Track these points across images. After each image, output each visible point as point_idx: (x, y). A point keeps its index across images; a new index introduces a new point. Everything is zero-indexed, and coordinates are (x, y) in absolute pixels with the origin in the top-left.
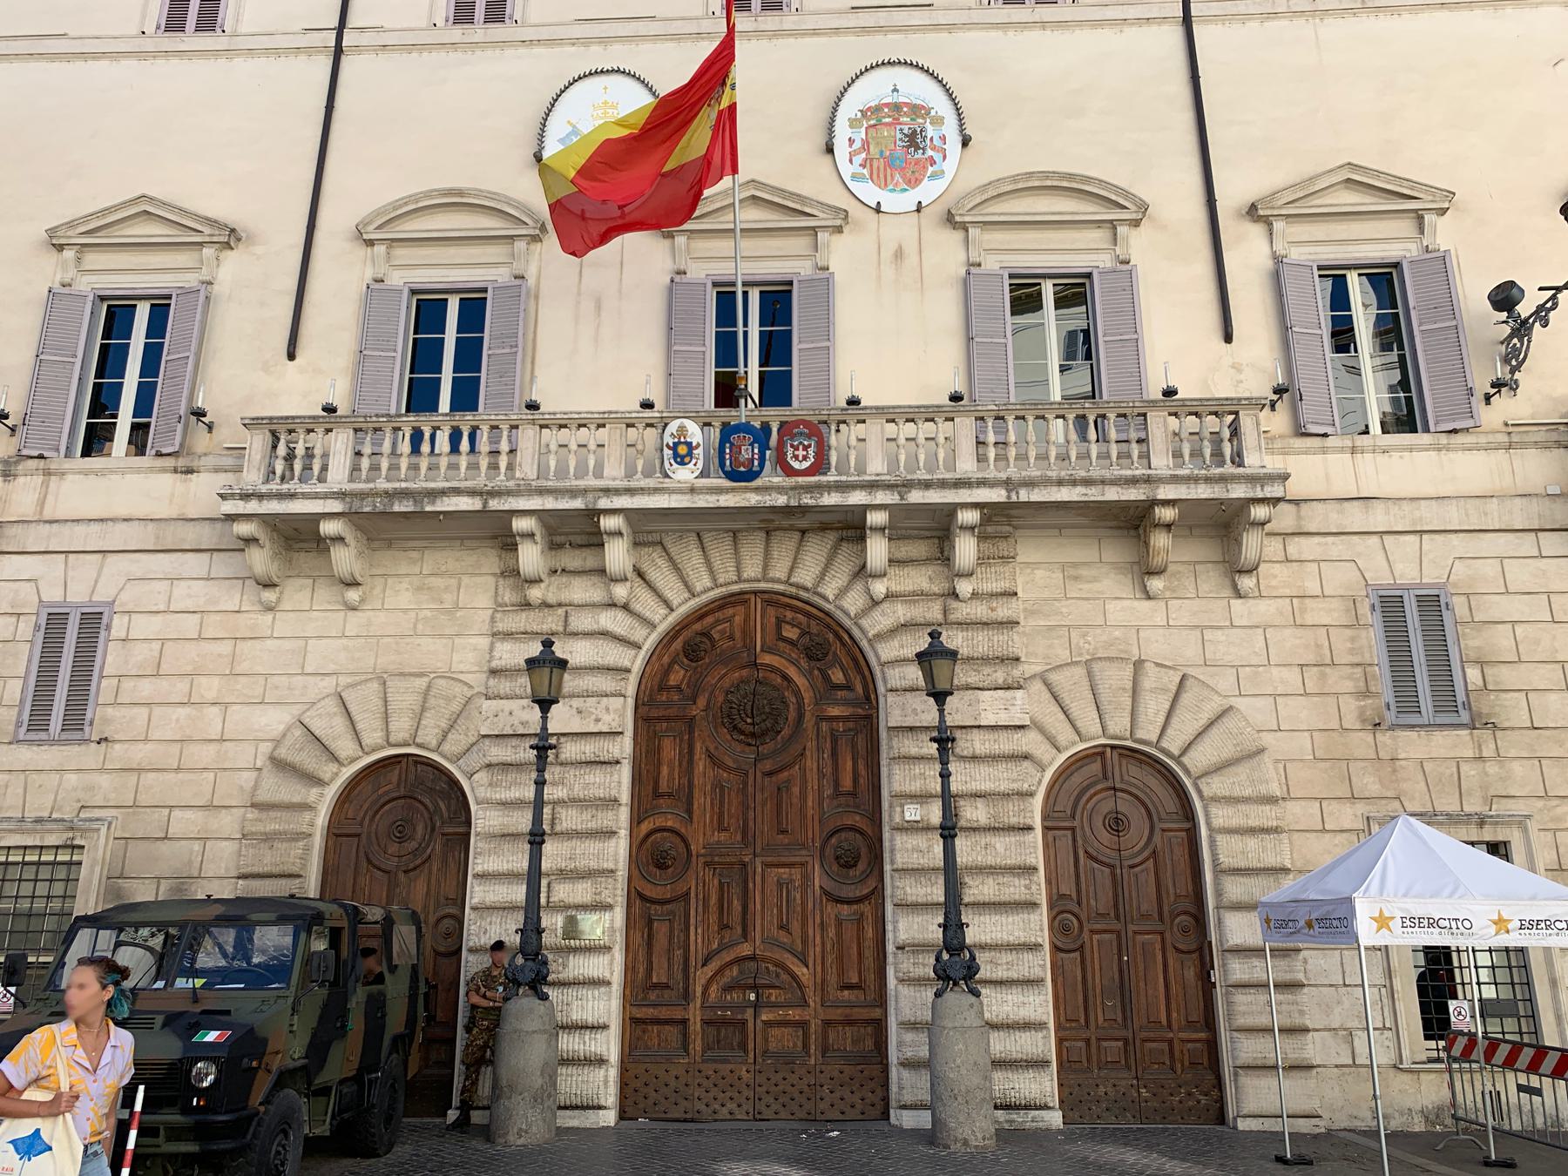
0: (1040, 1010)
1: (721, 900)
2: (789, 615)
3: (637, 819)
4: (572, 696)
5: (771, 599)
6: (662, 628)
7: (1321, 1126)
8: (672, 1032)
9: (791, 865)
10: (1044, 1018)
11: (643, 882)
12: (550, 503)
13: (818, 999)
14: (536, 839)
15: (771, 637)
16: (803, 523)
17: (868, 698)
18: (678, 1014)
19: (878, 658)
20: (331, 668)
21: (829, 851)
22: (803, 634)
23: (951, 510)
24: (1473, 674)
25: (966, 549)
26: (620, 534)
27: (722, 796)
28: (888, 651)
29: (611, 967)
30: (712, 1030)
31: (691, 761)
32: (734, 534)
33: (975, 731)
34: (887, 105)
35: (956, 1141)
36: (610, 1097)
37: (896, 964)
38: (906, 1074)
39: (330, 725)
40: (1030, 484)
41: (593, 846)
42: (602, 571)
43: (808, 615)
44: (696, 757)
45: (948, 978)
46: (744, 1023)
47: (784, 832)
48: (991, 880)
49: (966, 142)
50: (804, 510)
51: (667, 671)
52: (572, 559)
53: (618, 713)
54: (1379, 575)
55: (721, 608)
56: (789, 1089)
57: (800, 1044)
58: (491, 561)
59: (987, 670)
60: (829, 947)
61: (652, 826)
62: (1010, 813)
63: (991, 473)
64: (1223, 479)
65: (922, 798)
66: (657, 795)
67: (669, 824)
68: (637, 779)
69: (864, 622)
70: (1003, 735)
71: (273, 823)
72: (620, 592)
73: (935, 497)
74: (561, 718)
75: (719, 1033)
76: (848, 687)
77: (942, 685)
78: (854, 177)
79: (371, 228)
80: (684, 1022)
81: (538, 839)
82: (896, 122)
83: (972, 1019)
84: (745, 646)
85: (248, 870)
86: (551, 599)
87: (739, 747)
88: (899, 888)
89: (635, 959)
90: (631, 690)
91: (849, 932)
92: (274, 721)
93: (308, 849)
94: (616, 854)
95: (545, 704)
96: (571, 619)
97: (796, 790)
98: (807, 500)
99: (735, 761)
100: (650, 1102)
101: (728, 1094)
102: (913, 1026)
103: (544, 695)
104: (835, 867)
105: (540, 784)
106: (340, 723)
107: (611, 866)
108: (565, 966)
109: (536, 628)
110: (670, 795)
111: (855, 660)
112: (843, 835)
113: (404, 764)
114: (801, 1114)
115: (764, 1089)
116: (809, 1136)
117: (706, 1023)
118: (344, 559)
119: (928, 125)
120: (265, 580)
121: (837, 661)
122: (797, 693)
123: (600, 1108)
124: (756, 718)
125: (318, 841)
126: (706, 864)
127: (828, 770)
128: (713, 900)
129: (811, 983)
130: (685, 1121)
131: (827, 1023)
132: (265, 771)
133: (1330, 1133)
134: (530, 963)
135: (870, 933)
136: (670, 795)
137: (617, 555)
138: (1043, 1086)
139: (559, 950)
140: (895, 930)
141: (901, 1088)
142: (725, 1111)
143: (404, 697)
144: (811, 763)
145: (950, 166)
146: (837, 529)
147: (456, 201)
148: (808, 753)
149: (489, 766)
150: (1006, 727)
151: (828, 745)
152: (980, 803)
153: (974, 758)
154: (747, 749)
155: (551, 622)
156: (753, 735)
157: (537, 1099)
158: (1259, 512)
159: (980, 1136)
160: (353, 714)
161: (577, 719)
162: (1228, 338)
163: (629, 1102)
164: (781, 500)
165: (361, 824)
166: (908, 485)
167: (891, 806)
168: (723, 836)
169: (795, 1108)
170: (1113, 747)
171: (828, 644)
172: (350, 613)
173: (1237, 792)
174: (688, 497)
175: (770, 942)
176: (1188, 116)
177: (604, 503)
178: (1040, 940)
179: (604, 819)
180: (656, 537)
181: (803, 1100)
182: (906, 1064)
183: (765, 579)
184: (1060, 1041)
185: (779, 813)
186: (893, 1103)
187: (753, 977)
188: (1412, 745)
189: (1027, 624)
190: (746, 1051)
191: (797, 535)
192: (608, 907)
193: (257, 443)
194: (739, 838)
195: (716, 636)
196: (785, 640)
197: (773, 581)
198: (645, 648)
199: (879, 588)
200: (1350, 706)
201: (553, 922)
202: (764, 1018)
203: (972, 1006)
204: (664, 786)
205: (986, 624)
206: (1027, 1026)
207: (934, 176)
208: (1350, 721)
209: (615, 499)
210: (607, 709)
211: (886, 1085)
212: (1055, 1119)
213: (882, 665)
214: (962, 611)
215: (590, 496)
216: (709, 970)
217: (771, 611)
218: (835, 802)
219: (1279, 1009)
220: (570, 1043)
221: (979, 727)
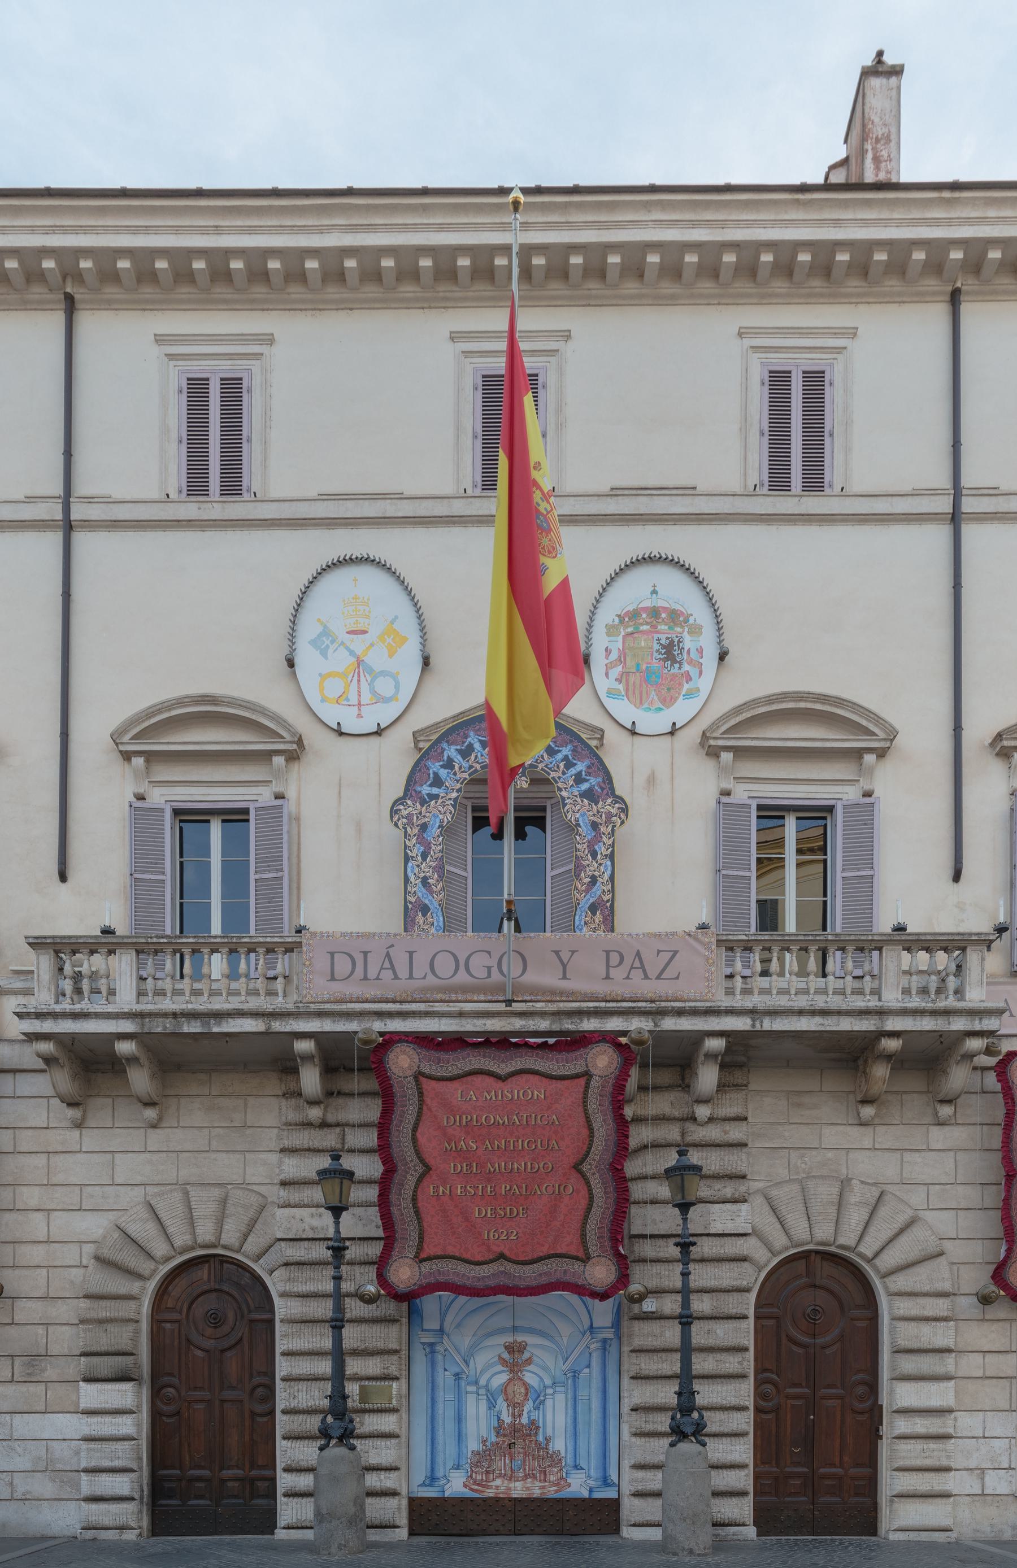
0: (745, 1455)
7: (953, 1536)
10: (747, 1461)
12: (327, 1026)
20: (138, 1179)
25: (707, 1077)
33: (704, 1238)
34: (645, 609)
36: (403, 1520)
39: (144, 1230)
40: (774, 1013)
58: (274, 1085)
62: (731, 1304)
63: (739, 1001)
64: (947, 1013)
71: (105, 1310)
73: (685, 1024)
78: (611, 693)
79: (126, 738)
82: (654, 629)
85: (88, 1349)
86: (331, 1118)
92: (94, 1226)
93: (137, 1332)
95: (337, 1211)
106: (151, 1227)
108: (362, 1424)
113: (212, 1262)
118: (140, 1080)
119: (687, 637)
120: (146, 1100)
123: (398, 1527)
125: (145, 1326)
132: (91, 1267)
133: (957, 1542)
138: (743, 1509)
143: (205, 1205)
145: (705, 683)
149: (287, 1264)
153: (702, 1260)
159: (702, 1547)
160: (163, 1219)
162: (957, 877)
165: (180, 1313)
166: (663, 1013)
170: (817, 1252)
172: (150, 1131)
173: (918, 1288)
176: (944, 635)
178: (747, 1403)
184: (757, 1478)
189: (756, 1144)
193: (44, 964)
201: (352, 1389)
203: (700, 1453)
206: (732, 1466)
207: (690, 694)
209: (388, 1022)
212: (750, 1532)
219: (934, 1453)
220: (372, 1480)
221: (708, 1235)
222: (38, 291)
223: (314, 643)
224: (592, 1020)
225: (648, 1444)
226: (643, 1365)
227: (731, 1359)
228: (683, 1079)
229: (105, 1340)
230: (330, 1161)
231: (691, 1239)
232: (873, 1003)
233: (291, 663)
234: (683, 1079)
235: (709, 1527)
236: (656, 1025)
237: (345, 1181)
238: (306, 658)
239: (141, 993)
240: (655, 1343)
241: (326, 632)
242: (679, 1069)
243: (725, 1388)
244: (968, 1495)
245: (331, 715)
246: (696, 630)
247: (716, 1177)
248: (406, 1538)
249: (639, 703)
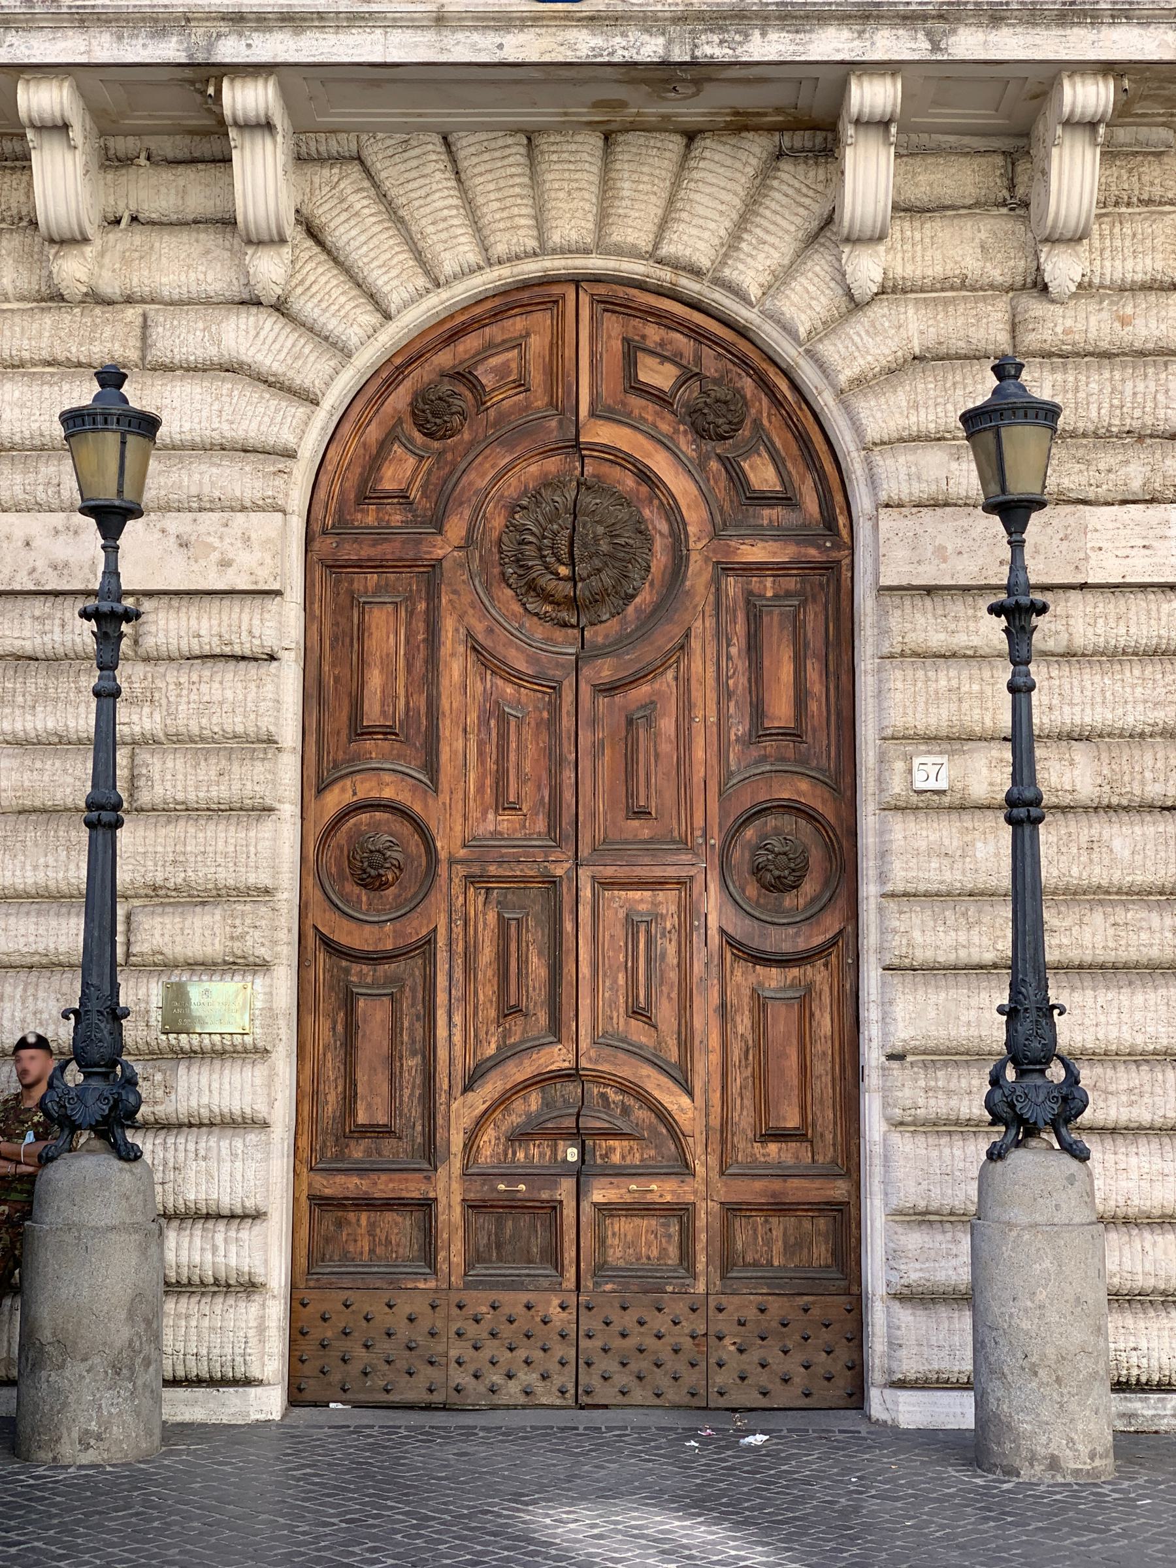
1: (502, 958)
2: (654, 334)
3: (316, 782)
4: (165, 508)
5: (615, 297)
6: (367, 358)
8: (400, 1229)
9: (658, 884)
11: (333, 917)
12: (104, 48)
13: (713, 1161)
14: (103, 816)
15: (612, 385)
16: (691, 112)
17: (830, 524)
18: (413, 1188)
19: (857, 428)
21: (738, 855)
22: (688, 376)
23: (1044, 80)
25: (1073, 176)
26: (267, 126)
27: (503, 736)
28: (882, 415)
29: (269, 1090)
30: (485, 1222)
31: (433, 661)
32: (531, 137)
33: (1074, 595)
35: (1032, 1459)
36: (271, 1362)
37: (885, 1091)
38: (905, 1316)
41: (222, 837)
42: (227, 222)
43: (697, 334)
44: (446, 650)
45: (1020, 1120)
46: (555, 1207)
47: (642, 814)
48: (1098, 917)
50: (699, 74)
51: (377, 459)
52: (156, 192)
53: (270, 548)
55: (497, 315)
56: (650, 1342)
57: (673, 1251)
59: (1106, 459)
60: (736, 1053)
61: (348, 798)
65: (955, 740)
66: (359, 731)
67: (388, 793)
68: (315, 694)
69: (830, 350)
70: (1137, 604)
72: (269, 269)
74: (145, 556)
75: (500, 1226)
76: (786, 499)
77: (1021, 485)
80: (426, 1206)
81: (107, 816)
83: (1072, 1210)
84: (552, 404)
86: (110, 286)
87: (539, 631)
88: (889, 931)
89: (316, 1079)
90: (297, 498)
91: (782, 1023)
94: (275, 855)
95: (111, 517)
96: (157, 332)
97: (667, 725)
98: (712, 48)
99: (532, 660)
100: (355, 1368)
101: (521, 1354)
102: (922, 1218)
103: (107, 493)
104: (752, 890)
105: (107, 695)
107: (263, 878)
108: (168, 1089)
109: (76, 350)
110: (387, 732)
111: (803, 440)
112: (771, 822)
114: (673, 1395)
115: (597, 1343)
116: (705, 1442)
117: (472, 1207)
121: (760, 434)
122: (672, 512)
123: (248, 1382)
124: (576, 563)
126: (471, 880)
127: (739, 682)
128: (487, 955)
129: (699, 1129)
130: (428, 1407)
131: (732, 1210)
134: (95, 1083)
135: (825, 1024)
136: (387, 732)
137: (261, 178)
139: (155, 1055)
140: (885, 1019)
141: (894, 1345)
142: (514, 1387)
144: (700, 665)
146: (771, 129)
148: (696, 644)
150: (1143, 587)
151: (740, 627)
152: (1080, 752)
153: (1069, 655)
154: (559, 634)
155: (111, 340)
156: (573, 603)
157: (121, 1369)
159: (1084, 1449)
161: (179, 557)
163: (309, 1369)
164: (650, 48)
167: (882, 759)
168: (506, 823)
169: (664, 1382)
171: (744, 398)
174: (430, 36)
175: (607, 1041)
177: (230, 50)
179: (247, 780)
180: (345, 144)
181: (682, 1368)
182: (909, 1296)
183: (601, 247)
185: (630, 773)
186: (876, 1375)
187: (576, 1114)
190: (558, 1266)
191: (676, 143)
192: (261, 966)
194: (541, 825)
195: (487, 380)
196: (638, 389)
197: (619, 251)
198: (327, 403)
199: (867, 268)
201: (140, 995)
202: (598, 1196)
203: (1071, 1179)
204: (373, 713)
205: (1106, 355)
209: (257, 39)
210: (246, 540)
211: (857, 1336)
213: (867, 448)
214: (1054, 324)
215: (199, 33)
216: (479, 1099)
217: (613, 326)
218: (755, 752)
220: (186, 1250)
221: (1083, 586)
224: (773, 36)
225: (934, 1154)
226: (917, 935)
227: (1154, 917)
228: (1012, 187)
230: (97, 388)
231: (1037, 596)
234: (1012, 187)
235: (1102, 1389)
236: (936, 47)
237: (130, 438)
240: (948, 876)
242: (999, 160)
243: (1139, 998)
244: (606, 1407)
247: (1103, 437)
248: (277, 1416)
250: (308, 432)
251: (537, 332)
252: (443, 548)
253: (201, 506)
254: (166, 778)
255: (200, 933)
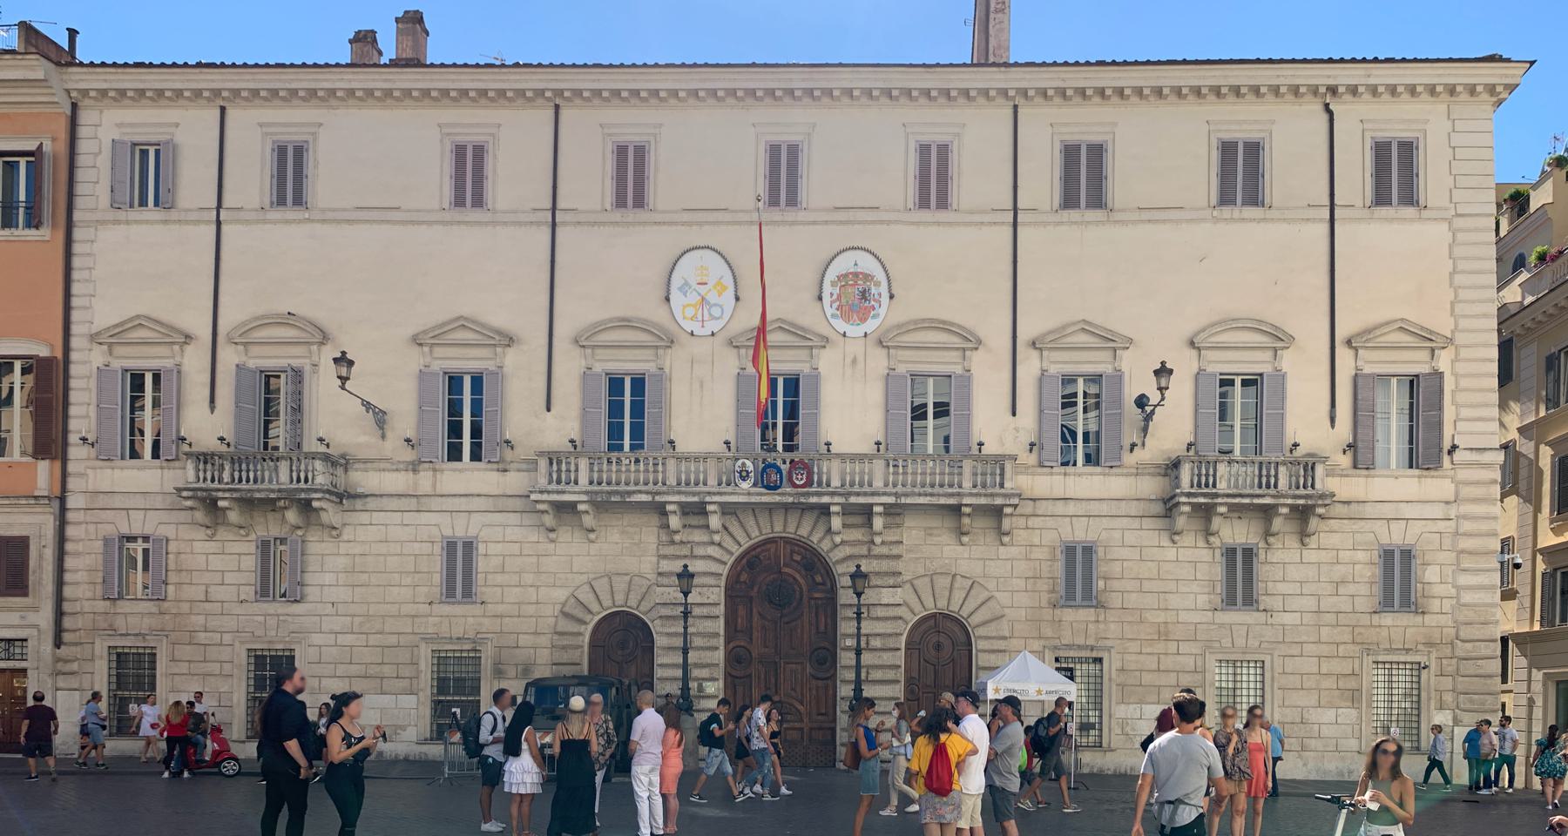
3: (727, 642)
12: (683, 499)
24: (1101, 583)
25: (878, 523)
39: (586, 596)
49: (892, 297)
51: (739, 575)
52: (694, 520)
53: (717, 595)
54: (1068, 536)
64: (992, 495)
68: (727, 623)
71: (566, 641)
72: (717, 538)
76: (823, 584)
90: (723, 584)
92: (561, 594)
95: (686, 594)
106: (591, 596)
125: (586, 649)
143: (620, 584)
145: (882, 311)
147: (625, 323)
158: (1320, 511)
162: (1014, 414)
171: (814, 563)
176: (1009, 284)
179: (713, 642)
188: (1069, 615)
199: (838, 539)
200: (1045, 597)
201: (693, 685)
207: (875, 316)
208: (1044, 603)
222: (540, 101)
223: (680, 289)
229: (565, 657)
232: (955, 490)
233: (668, 299)
238: (675, 296)
239: (591, 483)
241: (686, 283)
245: (688, 326)
246: (878, 284)
249: (847, 321)
250: (725, 570)
251: (772, 547)
252: (754, 593)
253: (704, 586)
254: (698, 642)
255: (704, 673)
